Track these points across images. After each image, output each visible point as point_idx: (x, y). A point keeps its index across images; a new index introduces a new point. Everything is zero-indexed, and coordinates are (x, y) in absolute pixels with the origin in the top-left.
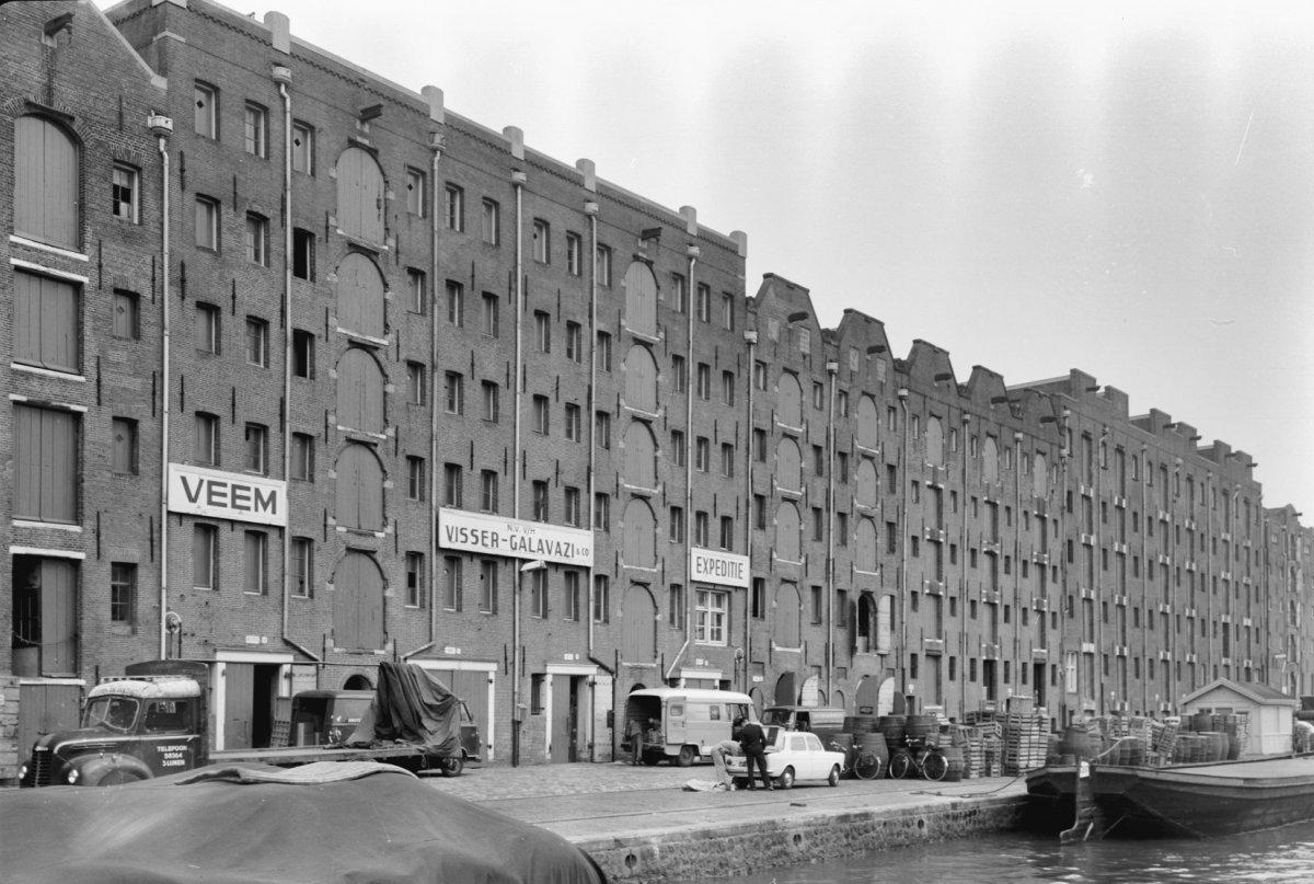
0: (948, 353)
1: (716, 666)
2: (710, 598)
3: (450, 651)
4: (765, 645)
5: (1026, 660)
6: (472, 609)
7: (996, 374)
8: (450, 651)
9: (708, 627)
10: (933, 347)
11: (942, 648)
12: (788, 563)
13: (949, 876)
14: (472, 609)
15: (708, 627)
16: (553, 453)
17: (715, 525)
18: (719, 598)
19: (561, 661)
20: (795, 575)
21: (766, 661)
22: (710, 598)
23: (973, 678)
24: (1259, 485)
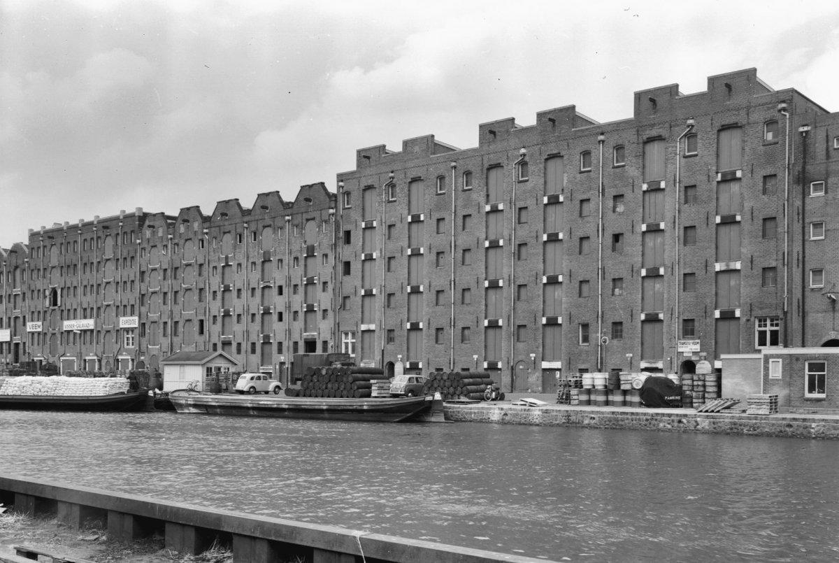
0: (750, 74)
1: (129, 354)
2: (130, 332)
3: (68, 355)
4: (145, 346)
5: (298, 339)
6: (71, 344)
7: (270, 193)
8: (68, 355)
9: (131, 341)
10: (264, 194)
11: (317, 337)
12: (154, 316)
13: (172, 437)
14: (71, 344)
15: (131, 341)
16: (89, 300)
17: (129, 308)
18: (132, 331)
19: (89, 355)
20: (156, 319)
21: (146, 351)
22: (130, 332)
23: (10, 353)
24: (712, 81)
